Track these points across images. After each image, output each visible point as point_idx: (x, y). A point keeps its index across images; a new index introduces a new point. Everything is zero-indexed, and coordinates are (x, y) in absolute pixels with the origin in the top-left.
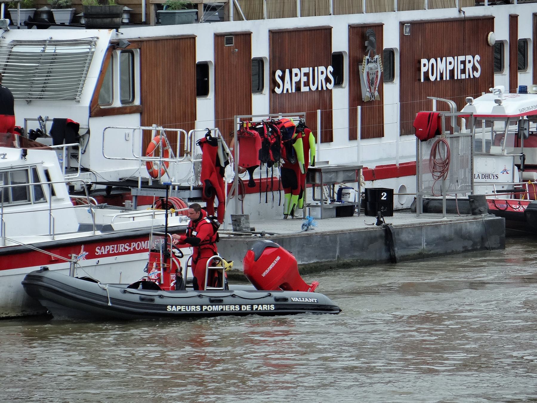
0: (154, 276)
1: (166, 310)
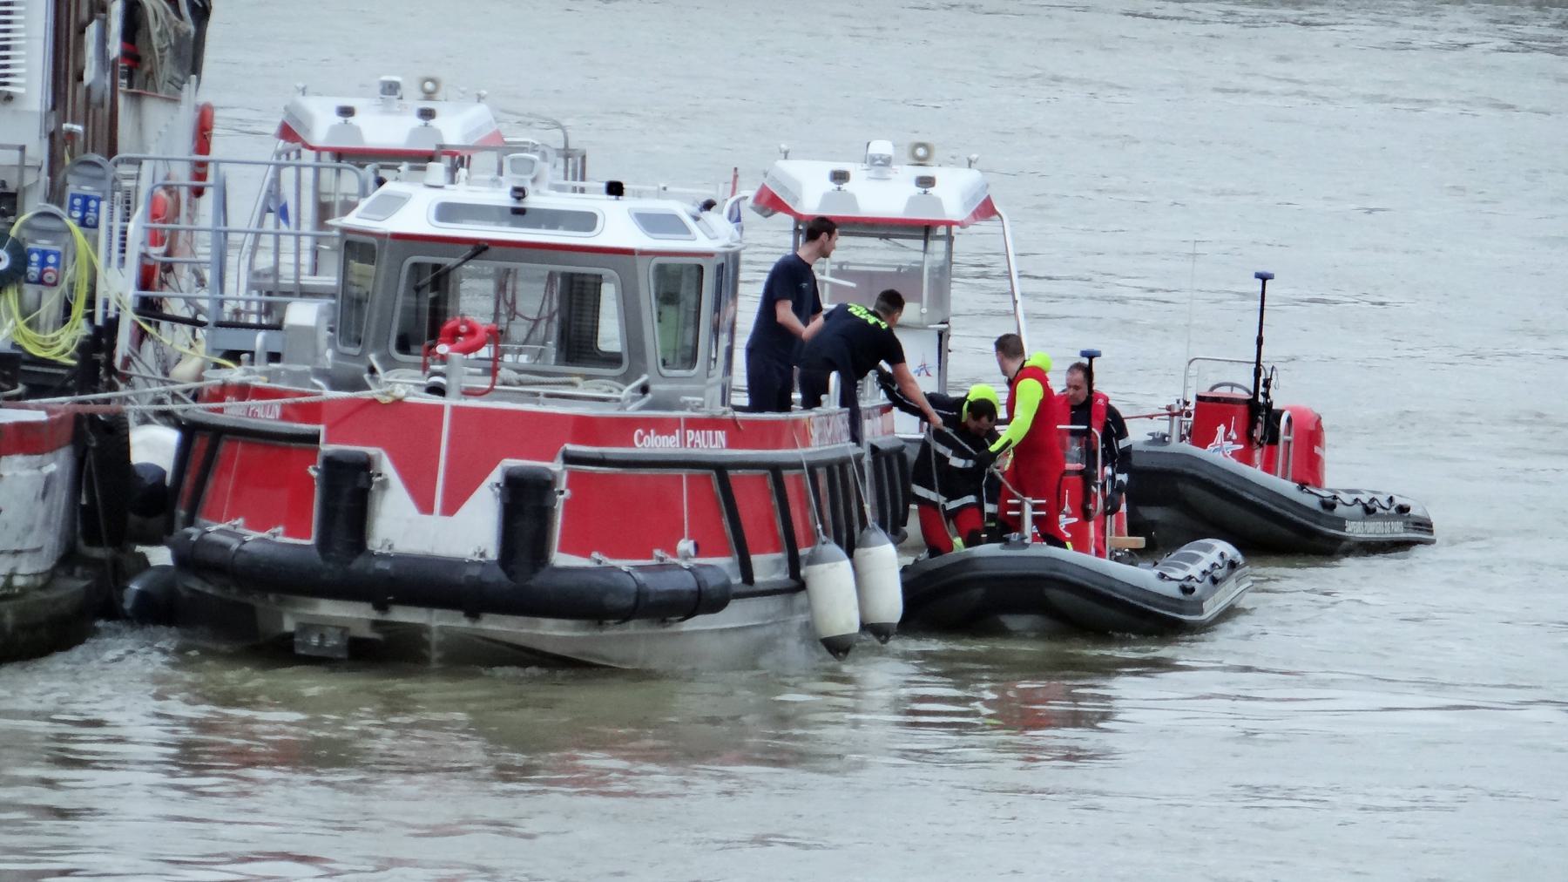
1: (1343, 529)
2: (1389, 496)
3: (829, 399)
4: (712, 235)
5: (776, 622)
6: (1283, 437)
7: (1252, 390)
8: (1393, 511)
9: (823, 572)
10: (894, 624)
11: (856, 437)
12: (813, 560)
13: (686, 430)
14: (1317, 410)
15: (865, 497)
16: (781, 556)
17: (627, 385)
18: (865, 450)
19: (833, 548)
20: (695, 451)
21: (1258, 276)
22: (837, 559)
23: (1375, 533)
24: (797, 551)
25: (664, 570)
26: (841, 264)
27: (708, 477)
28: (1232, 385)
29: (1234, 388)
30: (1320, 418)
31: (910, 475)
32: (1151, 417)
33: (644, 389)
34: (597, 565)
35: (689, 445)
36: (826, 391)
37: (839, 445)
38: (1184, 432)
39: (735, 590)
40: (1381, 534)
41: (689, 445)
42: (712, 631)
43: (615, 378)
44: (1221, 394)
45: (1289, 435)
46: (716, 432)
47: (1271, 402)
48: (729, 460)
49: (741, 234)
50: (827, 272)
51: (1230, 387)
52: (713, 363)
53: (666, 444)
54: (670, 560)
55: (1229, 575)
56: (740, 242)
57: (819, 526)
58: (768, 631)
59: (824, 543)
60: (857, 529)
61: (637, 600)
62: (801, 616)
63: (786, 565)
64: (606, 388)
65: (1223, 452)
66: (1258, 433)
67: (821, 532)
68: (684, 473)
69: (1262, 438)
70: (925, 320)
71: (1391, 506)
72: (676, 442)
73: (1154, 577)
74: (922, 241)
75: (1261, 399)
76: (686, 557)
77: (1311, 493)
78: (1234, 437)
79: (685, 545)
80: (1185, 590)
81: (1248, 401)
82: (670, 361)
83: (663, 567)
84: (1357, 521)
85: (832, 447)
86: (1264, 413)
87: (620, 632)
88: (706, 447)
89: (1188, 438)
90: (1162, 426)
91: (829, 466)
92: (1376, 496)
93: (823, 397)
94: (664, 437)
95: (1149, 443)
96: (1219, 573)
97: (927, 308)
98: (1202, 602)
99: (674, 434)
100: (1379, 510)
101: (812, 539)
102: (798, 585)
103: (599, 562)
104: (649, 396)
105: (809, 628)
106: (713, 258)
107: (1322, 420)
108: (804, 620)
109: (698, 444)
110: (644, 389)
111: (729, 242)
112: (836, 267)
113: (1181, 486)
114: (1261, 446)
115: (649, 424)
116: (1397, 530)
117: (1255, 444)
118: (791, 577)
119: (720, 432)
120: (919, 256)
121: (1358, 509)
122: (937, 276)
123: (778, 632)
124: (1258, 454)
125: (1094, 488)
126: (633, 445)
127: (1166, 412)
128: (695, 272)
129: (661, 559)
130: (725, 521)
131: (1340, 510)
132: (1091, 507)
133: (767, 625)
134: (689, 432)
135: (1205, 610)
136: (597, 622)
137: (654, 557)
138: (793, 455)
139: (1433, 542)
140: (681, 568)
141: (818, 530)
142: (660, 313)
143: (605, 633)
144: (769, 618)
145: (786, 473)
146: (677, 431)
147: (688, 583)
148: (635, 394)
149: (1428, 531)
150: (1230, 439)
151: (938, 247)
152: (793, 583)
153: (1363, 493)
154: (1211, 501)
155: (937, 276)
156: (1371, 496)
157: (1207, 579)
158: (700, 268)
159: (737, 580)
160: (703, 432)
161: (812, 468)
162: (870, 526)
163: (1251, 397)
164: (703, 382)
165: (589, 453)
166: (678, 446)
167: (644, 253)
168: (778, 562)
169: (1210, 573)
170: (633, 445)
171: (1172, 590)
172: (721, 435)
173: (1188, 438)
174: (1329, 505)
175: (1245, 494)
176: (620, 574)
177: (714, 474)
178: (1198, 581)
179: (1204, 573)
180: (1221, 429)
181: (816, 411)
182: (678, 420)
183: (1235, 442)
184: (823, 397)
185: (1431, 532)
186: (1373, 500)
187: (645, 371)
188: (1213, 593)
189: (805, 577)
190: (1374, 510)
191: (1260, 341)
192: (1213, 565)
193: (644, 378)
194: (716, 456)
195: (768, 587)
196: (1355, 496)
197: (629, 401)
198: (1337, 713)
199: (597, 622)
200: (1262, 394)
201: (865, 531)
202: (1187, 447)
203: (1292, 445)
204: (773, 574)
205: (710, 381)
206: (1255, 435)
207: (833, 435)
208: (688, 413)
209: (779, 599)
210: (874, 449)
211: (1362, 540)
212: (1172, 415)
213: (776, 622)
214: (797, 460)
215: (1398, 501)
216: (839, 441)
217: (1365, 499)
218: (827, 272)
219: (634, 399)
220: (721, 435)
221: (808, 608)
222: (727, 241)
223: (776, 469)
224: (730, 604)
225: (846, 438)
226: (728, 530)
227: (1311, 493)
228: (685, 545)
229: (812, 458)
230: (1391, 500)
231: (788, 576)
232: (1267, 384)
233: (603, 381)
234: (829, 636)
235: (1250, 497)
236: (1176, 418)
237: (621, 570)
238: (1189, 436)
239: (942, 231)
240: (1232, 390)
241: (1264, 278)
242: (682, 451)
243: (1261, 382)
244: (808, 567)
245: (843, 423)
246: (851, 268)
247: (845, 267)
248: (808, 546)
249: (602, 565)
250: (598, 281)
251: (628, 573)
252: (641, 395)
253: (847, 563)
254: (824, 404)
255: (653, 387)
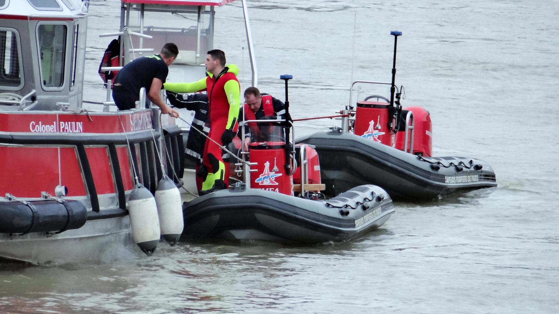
0: (269, 181)
1: (444, 181)
2: (470, 160)
3: (140, 103)
4: (71, 8)
5: (111, 234)
6: (408, 127)
7: (390, 100)
8: (472, 169)
9: (139, 204)
10: (177, 235)
11: (154, 123)
12: (133, 197)
13: (59, 121)
14: (427, 109)
15: (161, 159)
16: (115, 195)
17: (23, 96)
18: (160, 132)
19: (145, 191)
20: (65, 134)
21: (393, 33)
22: (146, 197)
23: (462, 182)
24: (124, 192)
25: (48, 204)
26: (149, 28)
27: (72, 149)
28: (378, 97)
29: (379, 99)
30: (429, 114)
31: (185, 145)
32: (331, 118)
33: (33, 98)
34: (9, 201)
35: (61, 131)
36: (138, 99)
37: (146, 130)
38: (350, 125)
39: (89, 215)
40: (465, 182)
41: (61, 131)
42: (75, 239)
43: (16, 92)
44: (371, 102)
45: (411, 125)
46: (77, 123)
47: (401, 107)
48: (83, 139)
49: (88, 8)
50: (142, 31)
51: (377, 98)
52: (72, 83)
53: (48, 130)
54: (51, 197)
55: (375, 206)
56: (87, 12)
57: (137, 178)
58: (107, 239)
59: (139, 187)
60: (156, 179)
61: (33, 222)
62: (126, 230)
63: (117, 200)
64: (11, 97)
65: (373, 136)
66: (393, 125)
67: (137, 181)
68: (59, 147)
69: (396, 128)
70: (198, 61)
71: (471, 166)
72: (54, 129)
73: (323, 205)
74: (197, 15)
75: (395, 105)
76: (60, 196)
77: (425, 161)
78: (380, 127)
79: (60, 189)
80: (342, 213)
81: (387, 106)
82: (47, 82)
83: (47, 202)
84: (451, 176)
85: (142, 131)
86: (397, 113)
87: (22, 240)
88: (71, 132)
89: (352, 128)
90: (337, 123)
91: (141, 143)
92: (463, 161)
93: (137, 102)
94: (47, 126)
95: (330, 133)
96: (369, 204)
97: (200, 53)
98: (354, 220)
99: (53, 124)
100: (465, 169)
101: (132, 185)
102: (124, 212)
103: (10, 199)
104: (36, 102)
105: (130, 239)
106: (73, 22)
107: (430, 115)
108: (127, 232)
109: (66, 130)
110: (33, 98)
111: (81, 12)
112: (146, 29)
113: (348, 158)
114: (395, 132)
115: (38, 119)
116: (474, 180)
117: (392, 131)
118: (120, 207)
119: (79, 123)
120: (195, 23)
121: (452, 169)
122: (205, 35)
123: (113, 239)
124: (394, 138)
125: (291, 155)
126: (30, 131)
127: (340, 114)
128: (62, 30)
129: (46, 197)
130: (83, 175)
131: (442, 170)
132: (289, 166)
133: (107, 235)
134: (61, 123)
135: (357, 225)
136: (9, 234)
137: (42, 196)
138: (120, 136)
139: (496, 186)
140: (58, 202)
141: (135, 180)
142: (42, 54)
143: (13, 240)
144: (107, 231)
145: (117, 146)
146: (55, 123)
147: (62, 211)
148: (28, 101)
149: (493, 179)
150: (377, 129)
151: (206, 18)
152: (121, 211)
153: (455, 159)
154: (366, 166)
155: (205, 35)
156: (460, 160)
157: (360, 207)
158: (65, 27)
159: (89, 209)
160: (69, 123)
161: (132, 143)
162: (165, 178)
163: (389, 104)
164: (68, 94)
165: (4, 135)
166: (55, 131)
167: (32, 18)
168: (112, 198)
169: (361, 204)
170: (30, 131)
171: (335, 213)
172: (80, 125)
173: (352, 128)
174: (435, 168)
175: (386, 163)
176: (22, 206)
177: (76, 147)
178: (352, 208)
179: (357, 203)
180: (372, 123)
181: (133, 111)
182: (55, 116)
183: (380, 131)
184: (137, 102)
185: (494, 180)
186: (461, 163)
187: (34, 88)
188: (363, 216)
189: (128, 207)
190: (462, 169)
191: (394, 71)
192: (365, 199)
193: (33, 91)
194: (77, 137)
195: (108, 213)
196: (450, 161)
197: (25, 105)
198: (73, 73)
199: (9, 234)
200: (396, 102)
201: (161, 181)
202: (351, 135)
203: (413, 131)
204: (110, 206)
205: (71, 93)
206: (391, 126)
207: (142, 124)
208: (61, 112)
209: (113, 220)
210: (165, 132)
211: (458, 187)
212: (344, 116)
213: (111, 234)
214: (123, 139)
215: (475, 163)
216: (146, 128)
217: (456, 163)
218: (142, 31)
219: (27, 104)
220: (80, 125)
221: (130, 225)
222: (80, 11)
223: (111, 144)
224: (86, 223)
225: (150, 126)
226: (84, 180)
227: (425, 161)
228: (60, 189)
229: (132, 138)
230: (471, 162)
231: (118, 206)
232: (398, 96)
233: (10, 93)
234: (143, 241)
235: (390, 164)
236: (346, 118)
237: (23, 204)
238: (353, 127)
239: (208, 8)
240: (378, 100)
241: (396, 35)
242: (58, 134)
243: (395, 95)
244: (130, 201)
245: (148, 117)
246: (155, 30)
247: (151, 30)
248: (130, 189)
249: (12, 201)
250: (5, 32)
251: (27, 205)
252: (31, 101)
253: (153, 198)
254: (137, 106)
255: (38, 97)
